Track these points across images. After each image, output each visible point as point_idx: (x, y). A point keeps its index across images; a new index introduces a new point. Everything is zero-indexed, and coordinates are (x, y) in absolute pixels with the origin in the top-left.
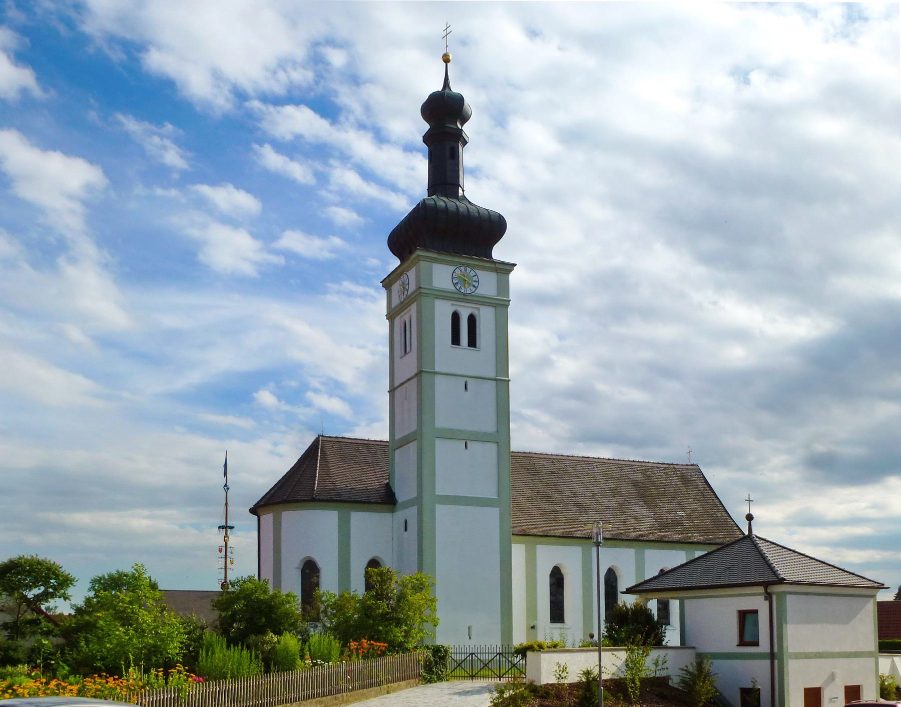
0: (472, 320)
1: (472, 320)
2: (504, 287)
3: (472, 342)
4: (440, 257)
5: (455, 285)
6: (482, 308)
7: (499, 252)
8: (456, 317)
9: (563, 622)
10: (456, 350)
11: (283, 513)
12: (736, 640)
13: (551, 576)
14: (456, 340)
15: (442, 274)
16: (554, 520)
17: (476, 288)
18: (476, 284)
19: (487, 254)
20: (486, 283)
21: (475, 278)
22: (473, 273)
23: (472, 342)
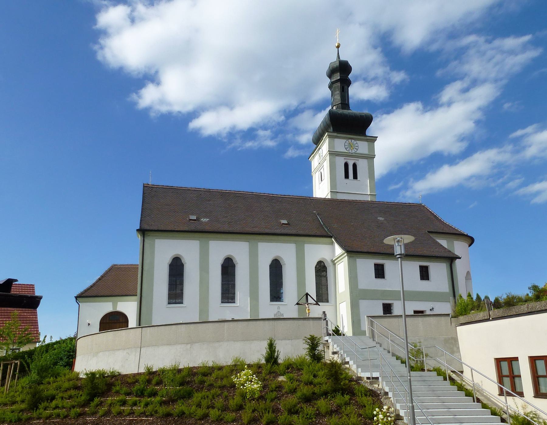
0: (355, 166)
1: (355, 166)
2: (372, 149)
3: (355, 177)
4: (339, 135)
5: (346, 149)
8: (346, 165)
9: (384, 304)
10: (347, 180)
11: (210, 241)
12: (400, 301)
13: (271, 266)
14: (347, 176)
15: (341, 144)
16: (163, 373)
17: (357, 150)
18: (357, 148)
20: (362, 147)
21: (357, 145)
22: (355, 142)
23: (355, 177)
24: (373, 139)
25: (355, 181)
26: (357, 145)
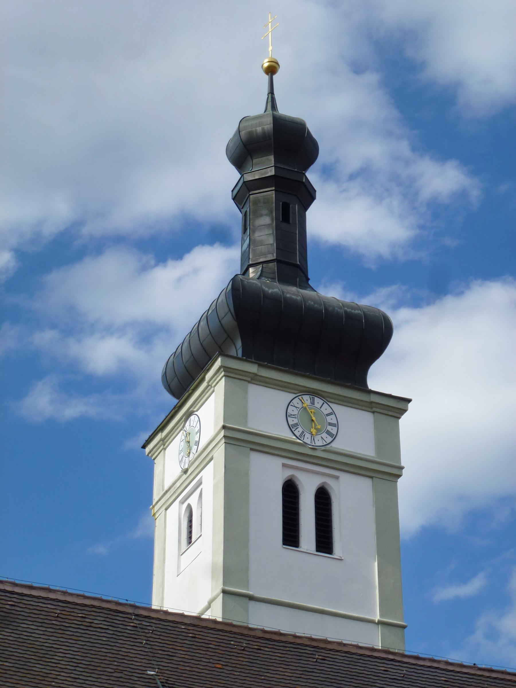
1: (323, 499)
2: (389, 441)
5: (291, 428)
6: (346, 479)
7: (381, 378)
8: (290, 492)
10: (289, 552)
14: (291, 536)
15: (272, 409)
17: (334, 437)
18: (334, 430)
19: (359, 382)
20: (353, 431)
21: (331, 419)
23: (325, 543)
24: (394, 407)
25: (323, 559)
26: (331, 419)
